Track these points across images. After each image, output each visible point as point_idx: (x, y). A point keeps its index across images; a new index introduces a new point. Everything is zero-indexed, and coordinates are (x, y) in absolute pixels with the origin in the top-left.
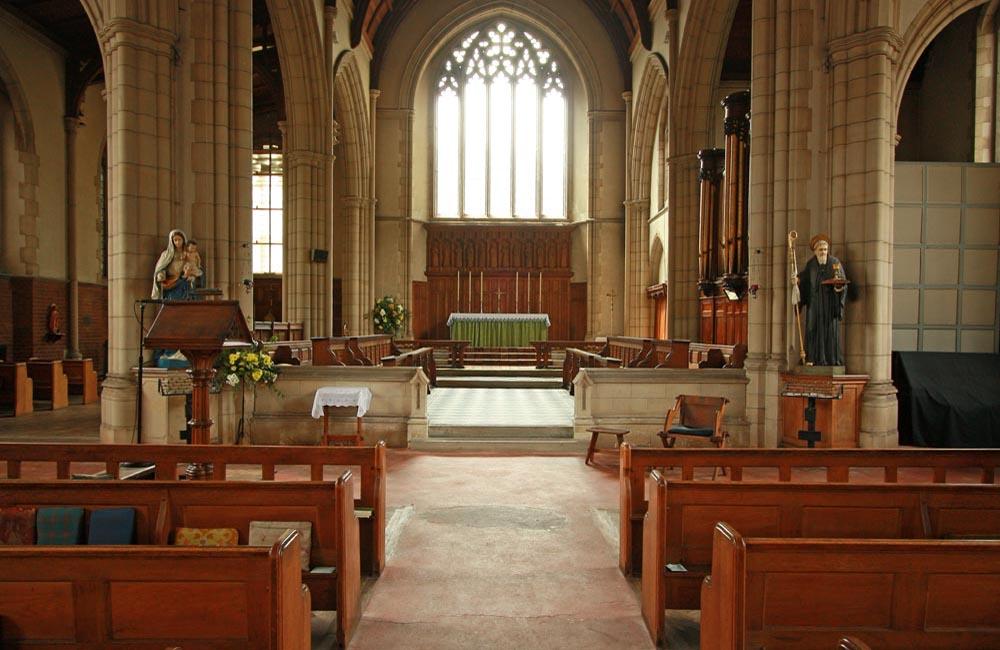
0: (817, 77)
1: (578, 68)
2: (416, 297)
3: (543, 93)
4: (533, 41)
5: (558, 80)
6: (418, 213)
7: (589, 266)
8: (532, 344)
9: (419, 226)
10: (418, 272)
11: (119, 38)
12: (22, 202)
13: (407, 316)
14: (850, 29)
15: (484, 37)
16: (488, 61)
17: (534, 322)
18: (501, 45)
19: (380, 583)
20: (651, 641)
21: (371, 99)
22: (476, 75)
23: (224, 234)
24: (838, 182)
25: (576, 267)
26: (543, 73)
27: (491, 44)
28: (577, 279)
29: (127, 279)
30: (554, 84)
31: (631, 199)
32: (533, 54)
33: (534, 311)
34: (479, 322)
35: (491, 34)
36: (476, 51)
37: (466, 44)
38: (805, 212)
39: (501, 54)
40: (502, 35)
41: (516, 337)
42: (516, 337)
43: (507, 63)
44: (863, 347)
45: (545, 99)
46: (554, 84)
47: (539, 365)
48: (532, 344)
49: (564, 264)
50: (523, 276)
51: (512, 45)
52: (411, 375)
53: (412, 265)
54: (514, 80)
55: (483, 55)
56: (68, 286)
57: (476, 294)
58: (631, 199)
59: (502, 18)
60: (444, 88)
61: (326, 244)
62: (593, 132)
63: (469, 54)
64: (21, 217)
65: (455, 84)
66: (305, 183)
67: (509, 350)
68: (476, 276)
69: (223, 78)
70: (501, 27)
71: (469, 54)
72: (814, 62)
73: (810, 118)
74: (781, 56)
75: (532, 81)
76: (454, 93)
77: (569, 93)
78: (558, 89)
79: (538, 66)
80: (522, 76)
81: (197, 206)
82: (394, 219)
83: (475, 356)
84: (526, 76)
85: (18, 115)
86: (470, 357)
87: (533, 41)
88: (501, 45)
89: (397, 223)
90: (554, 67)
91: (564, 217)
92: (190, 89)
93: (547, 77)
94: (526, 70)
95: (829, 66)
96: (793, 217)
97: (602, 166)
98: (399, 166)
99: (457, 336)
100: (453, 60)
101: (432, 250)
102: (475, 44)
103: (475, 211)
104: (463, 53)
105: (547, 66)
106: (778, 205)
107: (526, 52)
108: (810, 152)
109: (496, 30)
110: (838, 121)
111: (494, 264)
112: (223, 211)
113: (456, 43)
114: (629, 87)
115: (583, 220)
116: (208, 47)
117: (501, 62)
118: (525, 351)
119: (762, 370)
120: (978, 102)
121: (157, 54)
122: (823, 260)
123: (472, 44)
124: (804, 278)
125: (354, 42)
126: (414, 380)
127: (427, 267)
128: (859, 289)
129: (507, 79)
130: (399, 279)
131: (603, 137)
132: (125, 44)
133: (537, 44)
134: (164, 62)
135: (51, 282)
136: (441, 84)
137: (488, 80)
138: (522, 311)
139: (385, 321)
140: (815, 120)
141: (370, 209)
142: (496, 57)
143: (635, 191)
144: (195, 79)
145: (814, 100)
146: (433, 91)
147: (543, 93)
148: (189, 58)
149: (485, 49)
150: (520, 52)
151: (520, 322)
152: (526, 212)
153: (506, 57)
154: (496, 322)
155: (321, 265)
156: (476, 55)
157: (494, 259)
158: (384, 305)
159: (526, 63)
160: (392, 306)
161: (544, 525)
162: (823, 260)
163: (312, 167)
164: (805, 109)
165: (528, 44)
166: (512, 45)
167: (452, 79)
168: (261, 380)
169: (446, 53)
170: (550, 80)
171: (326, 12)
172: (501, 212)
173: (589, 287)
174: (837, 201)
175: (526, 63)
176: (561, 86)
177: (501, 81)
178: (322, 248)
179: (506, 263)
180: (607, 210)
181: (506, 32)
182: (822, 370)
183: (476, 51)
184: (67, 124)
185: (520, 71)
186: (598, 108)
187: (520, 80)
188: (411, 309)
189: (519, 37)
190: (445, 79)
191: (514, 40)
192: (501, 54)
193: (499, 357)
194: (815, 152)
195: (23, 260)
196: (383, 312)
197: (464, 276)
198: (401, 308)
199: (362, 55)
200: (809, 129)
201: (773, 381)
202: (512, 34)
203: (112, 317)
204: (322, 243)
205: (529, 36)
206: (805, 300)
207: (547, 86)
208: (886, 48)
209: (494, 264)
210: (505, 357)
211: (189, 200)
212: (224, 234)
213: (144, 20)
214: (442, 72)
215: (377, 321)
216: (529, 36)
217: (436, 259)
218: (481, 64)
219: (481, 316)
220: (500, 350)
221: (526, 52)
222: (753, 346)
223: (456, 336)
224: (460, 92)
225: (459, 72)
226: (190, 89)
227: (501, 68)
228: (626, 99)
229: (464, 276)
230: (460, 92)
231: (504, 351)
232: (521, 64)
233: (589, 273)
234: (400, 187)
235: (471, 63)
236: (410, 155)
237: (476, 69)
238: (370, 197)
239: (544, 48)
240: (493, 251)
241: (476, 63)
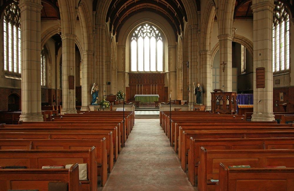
0: (199, 56)
1: (165, 35)
2: (127, 91)
3: (157, 41)
4: (155, 28)
5: (161, 38)
6: (127, 71)
7: (168, 83)
8: (154, 102)
9: (127, 73)
10: (127, 85)
11: (25, 7)
12: (50, 73)
13: (125, 96)
14: (203, 50)
15: (142, 27)
16: (143, 33)
17: (155, 96)
18: (147, 29)
19: (120, 155)
20: (182, 170)
21: (116, 44)
22: (141, 37)
23: (101, 83)
24: (202, 74)
25: (165, 83)
26: (157, 36)
27: (144, 29)
28: (166, 86)
29: (87, 91)
30: (160, 39)
31: (178, 67)
32: (155, 31)
33: (155, 94)
34: (142, 97)
35: (144, 27)
36: (141, 31)
37: (138, 29)
38: (197, 79)
39: (147, 31)
40: (147, 27)
41: (151, 100)
42: (151, 100)
43: (148, 34)
44: (205, 101)
45: (157, 42)
46: (160, 39)
47: (156, 106)
48: (154, 102)
49: (162, 82)
50: (153, 85)
51: (149, 29)
52: (132, 106)
53: (126, 83)
54: (150, 38)
55: (142, 32)
56: (56, 90)
57: (141, 90)
58: (178, 67)
59: (147, 23)
60: (133, 40)
61: (110, 81)
62: (169, 51)
63: (139, 31)
64: (50, 77)
65: (136, 39)
66: (106, 69)
67: (149, 103)
68: (141, 86)
69: (101, 58)
70: (147, 25)
71: (139, 31)
72: (198, 54)
73: (197, 64)
74: (193, 53)
75: (154, 38)
76: (135, 41)
77: (163, 41)
78: (161, 40)
79: (156, 34)
80: (152, 37)
81: (97, 78)
82: (122, 72)
83: (141, 105)
84: (153, 37)
85: (50, 57)
86: (140, 105)
87: (155, 28)
88: (147, 29)
89: (122, 73)
90: (160, 34)
91: (162, 71)
92: (96, 60)
93: (158, 37)
94: (153, 35)
95: (200, 55)
96: (195, 79)
97: (171, 59)
98: (122, 59)
99: (137, 100)
100: (135, 33)
101: (131, 79)
102: (140, 29)
103: (141, 70)
104: (138, 31)
105: (158, 34)
106: (193, 77)
107: (153, 31)
108: (198, 69)
109: (146, 26)
110: (201, 64)
111: (146, 82)
112: (101, 79)
113: (136, 29)
114: (177, 41)
115: (167, 72)
116: (98, 53)
117: (147, 33)
118: (153, 103)
119: (191, 105)
120: (242, 52)
121: (91, 55)
122: (199, 87)
123: (140, 29)
124: (196, 90)
125: (113, 35)
126: (132, 107)
127: (129, 83)
128: (205, 91)
129: (148, 38)
130: (123, 87)
131: (171, 52)
132: (87, 54)
133: (155, 29)
134: (92, 56)
135: (53, 89)
136: (132, 39)
137: (144, 38)
138: (152, 94)
139: (120, 97)
140: (198, 64)
141: (116, 70)
142: (146, 32)
143: (179, 66)
144: (96, 58)
145: (198, 60)
146: (130, 41)
147: (157, 41)
148: (96, 55)
149: (143, 30)
150: (151, 31)
151: (152, 96)
152: (153, 70)
153: (148, 32)
154: (146, 97)
155: (109, 85)
156: (141, 32)
157: (146, 81)
158: (120, 93)
159: (153, 34)
160: (121, 93)
161: (156, 136)
162: (199, 87)
163: (107, 65)
164: (197, 62)
165: (153, 29)
166: (149, 29)
167: (135, 38)
168: (108, 107)
169: (134, 32)
170: (159, 38)
171: (110, 32)
172: (147, 70)
173: (168, 88)
174: (202, 77)
175: (153, 34)
176: (161, 39)
177: (147, 38)
178: (109, 82)
179: (148, 82)
180: (173, 69)
181: (148, 26)
182: (198, 104)
183: (141, 31)
184: (56, 56)
185: (151, 36)
186: (170, 45)
187: (151, 38)
188: (125, 94)
189: (151, 27)
190: (133, 38)
191: (150, 28)
192: (147, 31)
193: (147, 105)
194: (198, 69)
195: (50, 85)
196: (119, 95)
197: (138, 86)
198: (123, 93)
199: (115, 37)
200: (197, 65)
201: (192, 106)
202: (149, 27)
203: (272, 100)
204: (109, 80)
205: (153, 27)
206: (196, 94)
207: (158, 39)
208: (228, 38)
209: (146, 82)
210: (148, 105)
211: (96, 77)
212: (101, 83)
213: (33, 2)
214: (132, 36)
215: (118, 97)
216: (153, 27)
217: (131, 81)
218: (142, 34)
219: (143, 95)
220: (147, 103)
221: (153, 31)
222: (190, 101)
223: (137, 100)
224: (137, 41)
225: (137, 36)
226: (96, 60)
227: (147, 35)
228: (177, 44)
229: (138, 86)
230: (137, 41)
231: (148, 103)
232: (152, 34)
233: (168, 85)
234: (123, 65)
235: (139, 34)
236: (125, 57)
237: (141, 35)
238: (116, 67)
239: (157, 30)
240: (145, 79)
241: (141, 34)
